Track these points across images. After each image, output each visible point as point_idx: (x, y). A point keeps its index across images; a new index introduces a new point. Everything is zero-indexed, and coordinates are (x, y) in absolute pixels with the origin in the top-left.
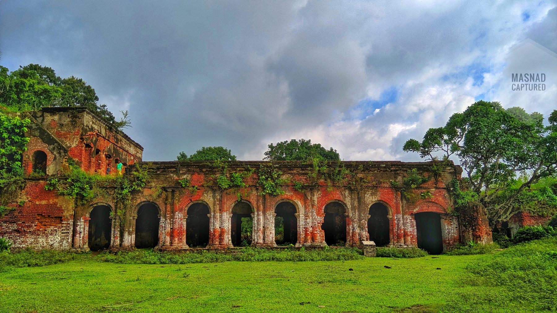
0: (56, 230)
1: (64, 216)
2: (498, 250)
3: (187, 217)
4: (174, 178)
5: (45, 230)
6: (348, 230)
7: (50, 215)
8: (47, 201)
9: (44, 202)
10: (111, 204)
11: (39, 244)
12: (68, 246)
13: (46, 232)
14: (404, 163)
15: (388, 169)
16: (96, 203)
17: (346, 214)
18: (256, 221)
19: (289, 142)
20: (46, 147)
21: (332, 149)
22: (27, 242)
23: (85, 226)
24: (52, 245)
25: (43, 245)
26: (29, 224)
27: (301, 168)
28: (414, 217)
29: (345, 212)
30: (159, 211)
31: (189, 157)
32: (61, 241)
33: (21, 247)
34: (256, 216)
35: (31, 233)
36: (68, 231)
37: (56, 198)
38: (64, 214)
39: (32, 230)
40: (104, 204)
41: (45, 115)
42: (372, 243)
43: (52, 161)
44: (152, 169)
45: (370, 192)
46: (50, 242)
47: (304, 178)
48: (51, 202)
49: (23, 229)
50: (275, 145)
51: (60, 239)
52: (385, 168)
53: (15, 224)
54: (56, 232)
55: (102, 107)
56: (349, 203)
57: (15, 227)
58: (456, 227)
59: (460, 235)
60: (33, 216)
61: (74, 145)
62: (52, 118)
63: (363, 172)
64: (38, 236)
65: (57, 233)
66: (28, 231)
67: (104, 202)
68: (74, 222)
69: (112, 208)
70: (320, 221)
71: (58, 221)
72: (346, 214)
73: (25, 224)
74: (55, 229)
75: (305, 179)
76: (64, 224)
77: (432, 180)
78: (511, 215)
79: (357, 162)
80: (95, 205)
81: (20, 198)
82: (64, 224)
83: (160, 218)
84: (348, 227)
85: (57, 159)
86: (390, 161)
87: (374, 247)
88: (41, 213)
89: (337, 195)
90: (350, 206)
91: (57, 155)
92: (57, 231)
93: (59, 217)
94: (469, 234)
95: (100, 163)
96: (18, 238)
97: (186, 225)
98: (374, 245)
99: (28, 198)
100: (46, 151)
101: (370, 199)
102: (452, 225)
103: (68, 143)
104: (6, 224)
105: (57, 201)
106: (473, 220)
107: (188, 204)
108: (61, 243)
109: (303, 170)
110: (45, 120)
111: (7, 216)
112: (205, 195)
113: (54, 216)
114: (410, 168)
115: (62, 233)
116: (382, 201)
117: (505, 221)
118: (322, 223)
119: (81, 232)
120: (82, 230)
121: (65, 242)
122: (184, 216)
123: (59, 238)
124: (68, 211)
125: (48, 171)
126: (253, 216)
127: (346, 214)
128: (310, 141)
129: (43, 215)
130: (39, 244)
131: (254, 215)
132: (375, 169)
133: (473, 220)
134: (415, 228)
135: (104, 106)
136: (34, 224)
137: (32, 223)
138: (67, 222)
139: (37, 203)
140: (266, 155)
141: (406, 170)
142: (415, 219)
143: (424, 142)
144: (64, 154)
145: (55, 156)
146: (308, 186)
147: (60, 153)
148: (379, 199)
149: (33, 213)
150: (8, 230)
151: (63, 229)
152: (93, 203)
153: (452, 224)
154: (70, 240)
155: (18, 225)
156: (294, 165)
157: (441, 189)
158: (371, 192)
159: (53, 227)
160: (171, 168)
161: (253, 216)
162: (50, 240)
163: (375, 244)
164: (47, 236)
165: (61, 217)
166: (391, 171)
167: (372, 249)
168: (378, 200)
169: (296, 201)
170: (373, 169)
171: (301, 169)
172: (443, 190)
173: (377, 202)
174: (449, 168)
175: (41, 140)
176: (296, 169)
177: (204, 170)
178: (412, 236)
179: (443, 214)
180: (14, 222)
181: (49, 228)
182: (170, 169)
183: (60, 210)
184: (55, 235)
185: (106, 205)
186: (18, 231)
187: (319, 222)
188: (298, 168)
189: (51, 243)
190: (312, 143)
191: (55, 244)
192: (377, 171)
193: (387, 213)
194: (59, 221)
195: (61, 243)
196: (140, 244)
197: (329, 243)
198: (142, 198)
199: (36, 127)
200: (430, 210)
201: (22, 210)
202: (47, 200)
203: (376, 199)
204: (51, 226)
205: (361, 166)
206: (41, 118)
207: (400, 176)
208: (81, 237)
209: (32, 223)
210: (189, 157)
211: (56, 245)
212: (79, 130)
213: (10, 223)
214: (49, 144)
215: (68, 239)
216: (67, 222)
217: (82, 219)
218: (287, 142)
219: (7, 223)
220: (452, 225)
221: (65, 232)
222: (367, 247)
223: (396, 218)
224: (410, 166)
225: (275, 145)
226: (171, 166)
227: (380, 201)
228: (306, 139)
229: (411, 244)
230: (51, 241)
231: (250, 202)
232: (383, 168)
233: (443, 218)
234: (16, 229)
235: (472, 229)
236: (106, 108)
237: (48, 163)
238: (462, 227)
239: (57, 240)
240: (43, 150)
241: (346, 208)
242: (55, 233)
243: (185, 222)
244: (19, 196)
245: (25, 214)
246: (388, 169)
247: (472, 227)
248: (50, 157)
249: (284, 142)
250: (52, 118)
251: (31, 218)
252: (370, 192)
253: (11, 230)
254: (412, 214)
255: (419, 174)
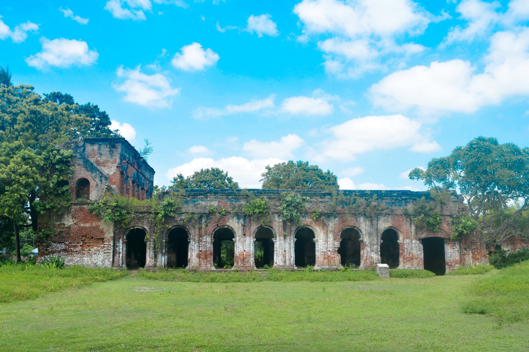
0: (99, 250)
1: (106, 238)
2: (495, 271)
3: (213, 241)
4: (202, 205)
5: (89, 250)
6: (362, 254)
7: (93, 236)
8: (90, 224)
9: (87, 225)
10: (146, 227)
11: (85, 263)
12: (110, 265)
13: (90, 252)
14: (414, 192)
15: (399, 198)
16: (133, 227)
17: (361, 239)
18: (278, 246)
19: (286, 164)
20: (89, 175)
21: (329, 173)
22: (74, 261)
23: (123, 247)
24: (95, 263)
25: (88, 263)
26: (75, 244)
27: (320, 196)
28: (421, 242)
29: (360, 238)
30: (189, 234)
31: (185, 178)
32: (103, 260)
33: (69, 265)
34: (277, 240)
35: (77, 252)
36: (110, 252)
37: (98, 222)
38: (106, 236)
39: (77, 249)
40: (140, 228)
41: (86, 146)
42: (386, 265)
43: (94, 188)
44: (183, 196)
45: (383, 219)
46: (94, 261)
47: (323, 205)
48: (94, 224)
49: (70, 249)
50: (272, 166)
51: (102, 258)
52: (396, 196)
53: (63, 244)
54: (99, 252)
55: (115, 131)
56: (364, 229)
57: (63, 246)
58: (458, 251)
59: (461, 258)
60: (78, 238)
61: (111, 173)
62: (92, 148)
63: (376, 201)
64: (83, 256)
65: (100, 253)
66: (75, 250)
67: (140, 225)
68: (114, 244)
69: (147, 231)
70: (337, 246)
71: (100, 242)
72: (360, 239)
73: (71, 244)
74: (98, 249)
75: (324, 207)
76: (105, 244)
77: (438, 208)
78: (505, 239)
79: (371, 191)
80: (132, 228)
81: (67, 221)
82: (105, 244)
83: (190, 242)
84: (362, 251)
85: (99, 186)
86: (402, 191)
87: (387, 269)
88: (85, 235)
89: (351, 222)
90: (365, 232)
91: (99, 182)
92: (100, 251)
93: (101, 239)
94: (469, 257)
95: (129, 188)
96: (66, 256)
97: (213, 248)
98: (388, 268)
99: (73, 221)
100: (90, 178)
101: (384, 224)
102: (454, 249)
103: (106, 171)
104: (55, 244)
105: (99, 224)
106: (473, 244)
107: (215, 228)
108: (103, 262)
109: (321, 198)
110: (86, 150)
111: (56, 237)
112: (231, 220)
113: (96, 238)
114: (419, 197)
115: (104, 253)
116: (394, 227)
117: (499, 244)
118: (339, 248)
119: (120, 253)
120: (121, 251)
121: (107, 261)
122: (211, 240)
123: (102, 257)
124: (109, 233)
125: (91, 196)
126: (275, 241)
127: (361, 239)
128: (307, 163)
129: (87, 236)
130: (85, 263)
131: (276, 240)
132: (388, 198)
133: (473, 244)
134: (423, 251)
135: (117, 130)
136: (79, 245)
137: (77, 243)
138: (108, 243)
139: (82, 225)
140: (263, 176)
141: (415, 199)
142: (422, 243)
143: (429, 170)
144: (105, 181)
145: (97, 183)
146: (327, 213)
147: (101, 180)
148: (391, 225)
149: (78, 235)
150: (57, 250)
151: (105, 249)
152: (130, 226)
153: (454, 247)
154: (111, 260)
155: (65, 245)
156: (314, 193)
157: (445, 216)
158: (384, 219)
159: (96, 247)
160: (199, 195)
161: (275, 241)
162: (93, 259)
163: (388, 267)
164: (91, 255)
165: (103, 239)
166: (402, 199)
167: (386, 271)
168: (390, 227)
169: (315, 227)
170: (386, 198)
171: (320, 197)
172: (447, 217)
173: (389, 228)
174: (453, 197)
175: (84, 168)
176: (315, 197)
177: (230, 197)
178: (419, 259)
179: (446, 238)
180: (62, 243)
181: (93, 248)
182: (198, 197)
183: (102, 232)
184: (99, 255)
185: (142, 228)
186: (65, 250)
187: (336, 247)
188: (318, 196)
189: (95, 262)
190: (310, 164)
191: (98, 263)
192: (390, 200)
193: (397, 238)
194: (101, 242)
195: (103, 262)
196: (170, 265)
197: (258, 266)
198: (173, 223)
199: (80, 157)
200: (430, 236)
201: (68, 232)
202: (91, 223)
203: (388, 226)
204: (95, 246)
205: (375, 196)
206: (82, 148)
207: (410, 204)
208: (121, 257)
209: (77, 243)
210: (185, 178)
211: (100, 263)
212: (116, 159)
213: (59, 243)
214: (92, 172)
215: (110, 258)
216: (108, 243)
217: (120, 241)
218: (284, 163)
219: (56, 243)
220: (454, 249)
221: (106, 252)
222: (382, 269)
223: (405, 243)
224: (419, 195)
225: (272, 166)
226: (200, 194)
227: (391, 227)
228: (304, 161)
229: (418, 265)
230: (95, 260)
231: (272, 228)
232: (395, 197)
233: (447, 243)
234: (64, 248)
235: (472, 252)
236: (119, 132)
237: (91, 189)
238: (463, 250)
239: (100, 259)
240: (86, 178)
241: (361, 233)
242: (98, 253)
243: (212, 246)
244: (66, 219)
245: (72, 235)
246: (399, 198)
247: (472, 251)
248: (92, 183)
249: (282, 163)
250: (92, 148)
251: (77, 239)
252: (383, 219)
253: (59, 250)
254: (419, 240)
255: (427, 202)
